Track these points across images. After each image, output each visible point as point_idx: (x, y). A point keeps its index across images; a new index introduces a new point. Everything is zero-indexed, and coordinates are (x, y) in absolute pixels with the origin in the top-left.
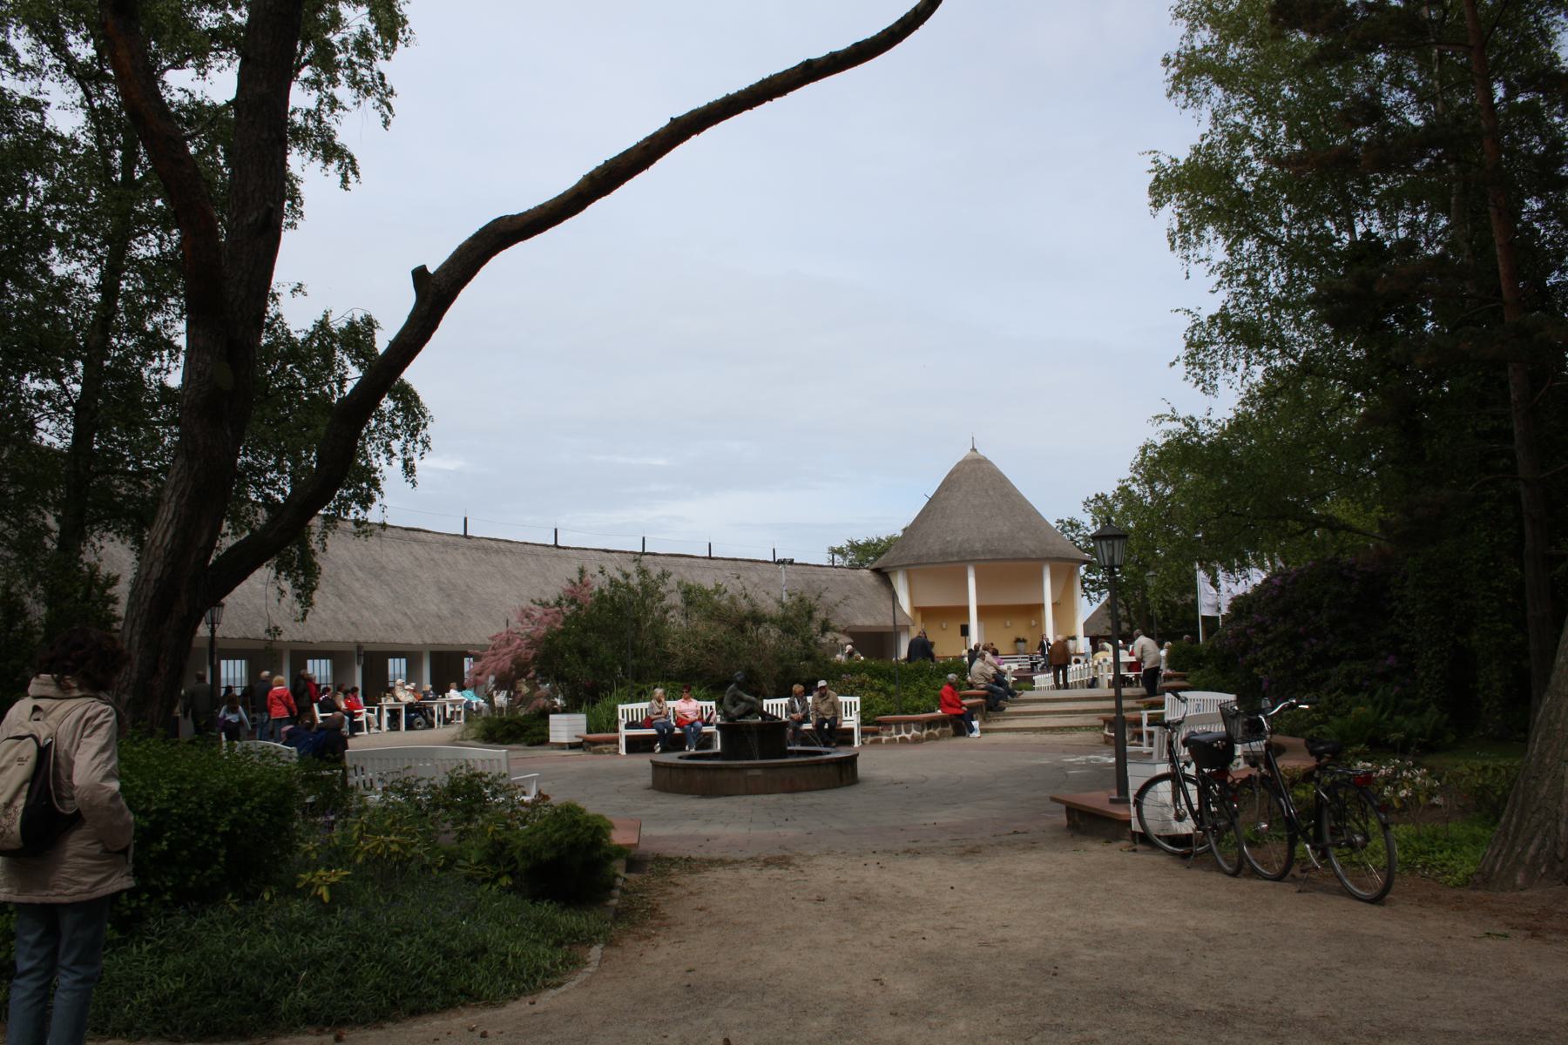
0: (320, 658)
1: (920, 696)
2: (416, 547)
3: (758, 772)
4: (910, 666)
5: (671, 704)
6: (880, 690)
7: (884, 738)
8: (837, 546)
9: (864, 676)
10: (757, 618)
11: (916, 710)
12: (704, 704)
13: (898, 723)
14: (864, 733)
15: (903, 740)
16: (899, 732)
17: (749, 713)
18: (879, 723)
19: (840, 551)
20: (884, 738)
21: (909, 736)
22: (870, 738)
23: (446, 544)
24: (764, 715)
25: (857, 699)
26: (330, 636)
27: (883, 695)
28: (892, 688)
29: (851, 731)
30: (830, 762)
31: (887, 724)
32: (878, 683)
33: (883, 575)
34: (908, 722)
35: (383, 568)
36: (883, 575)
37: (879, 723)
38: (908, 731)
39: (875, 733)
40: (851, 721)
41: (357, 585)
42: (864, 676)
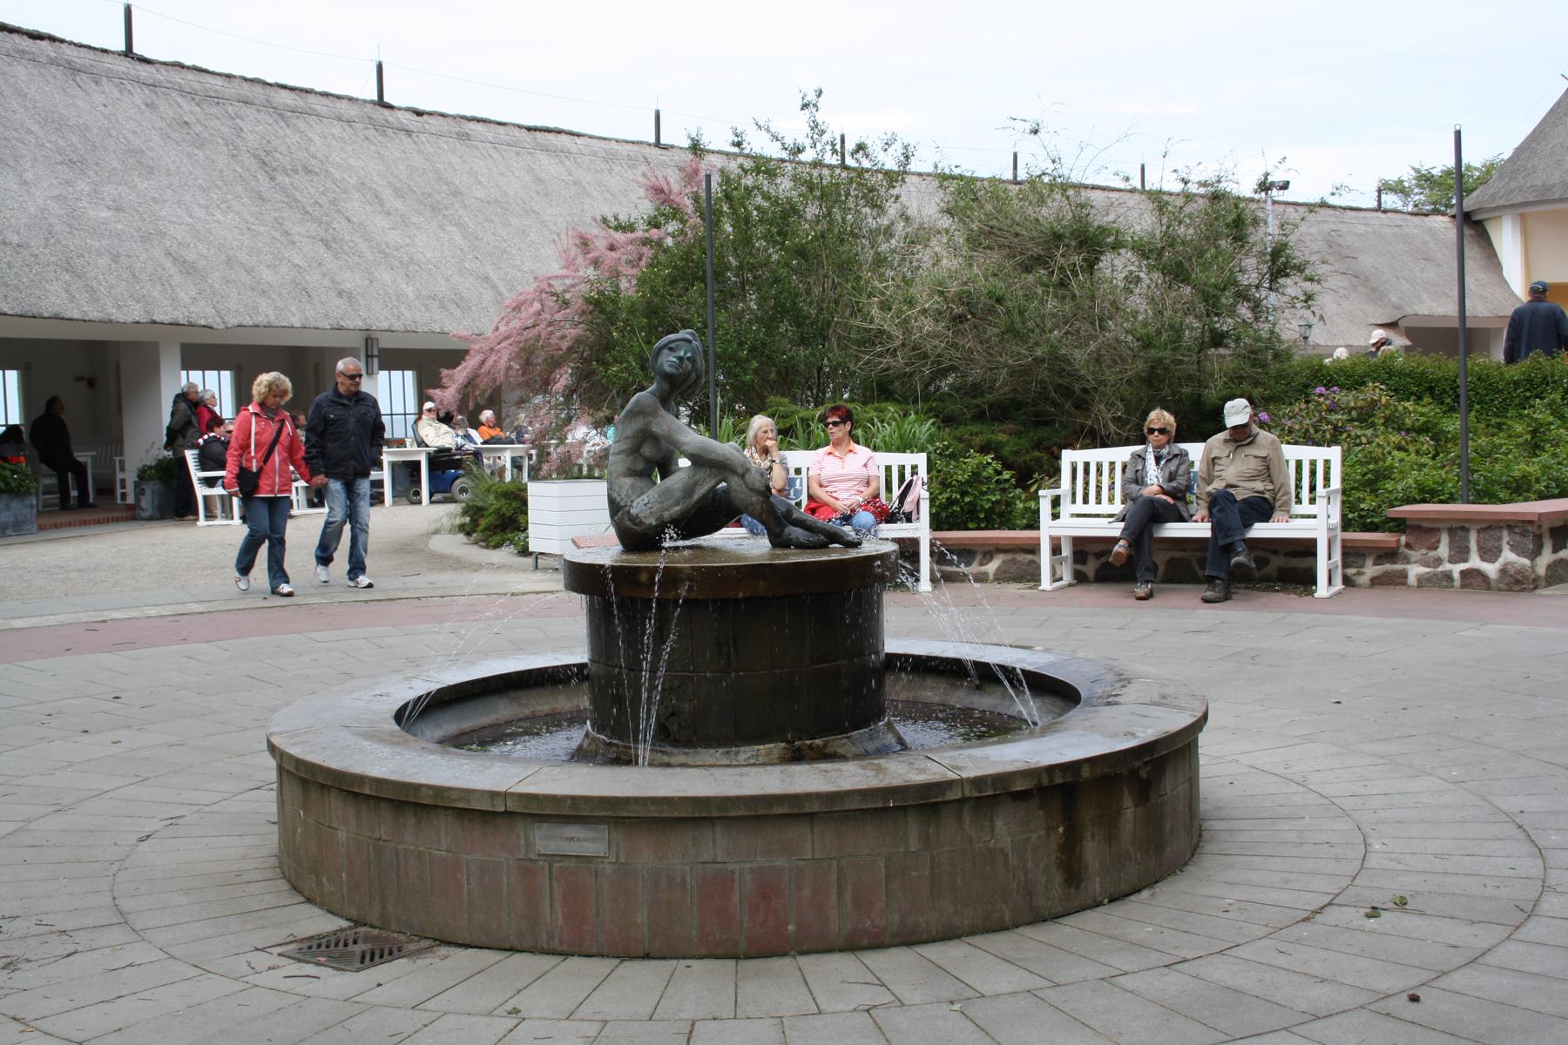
0: (403, 368)
1: (1534, 448)
2: (544, 158)
3: (586, 842)
4: (1515, 372)
5: (797, 458)
6: (1423, 429)
7: (1415, 571)
8: (1392, 177)
9: (1374, 391)
10: (1090, 242)
11: (1520, 489)
12: (896, 459)
13: (1458, 529)
14: (1352, 554)
15: (1473, 579)
16: (1460, 554)
17: (709, 513)
18: (1400, 525)
19: (1398, 188)
20: (1415, 571)
21: (1491, 569)
22: (1371, 570)
23: (611, 158)
24: (775, 518)
25: (1334, 453)
26: (266, 313)
27: (1426, 443)
28: (1452, 425)
29: (1306, 548)
30: (995, 794)
31: (1424, 531)
32: (1415, 411)
33: (1473, 226)
34: (1491, 527)
35: (456, 193)
36: (1473, 226)
37: (1400, 525)
38: (1489, 554)
39: (1390, 554)
40: (1314, 519)
41: (382, 222)
42: (1374, 391)
